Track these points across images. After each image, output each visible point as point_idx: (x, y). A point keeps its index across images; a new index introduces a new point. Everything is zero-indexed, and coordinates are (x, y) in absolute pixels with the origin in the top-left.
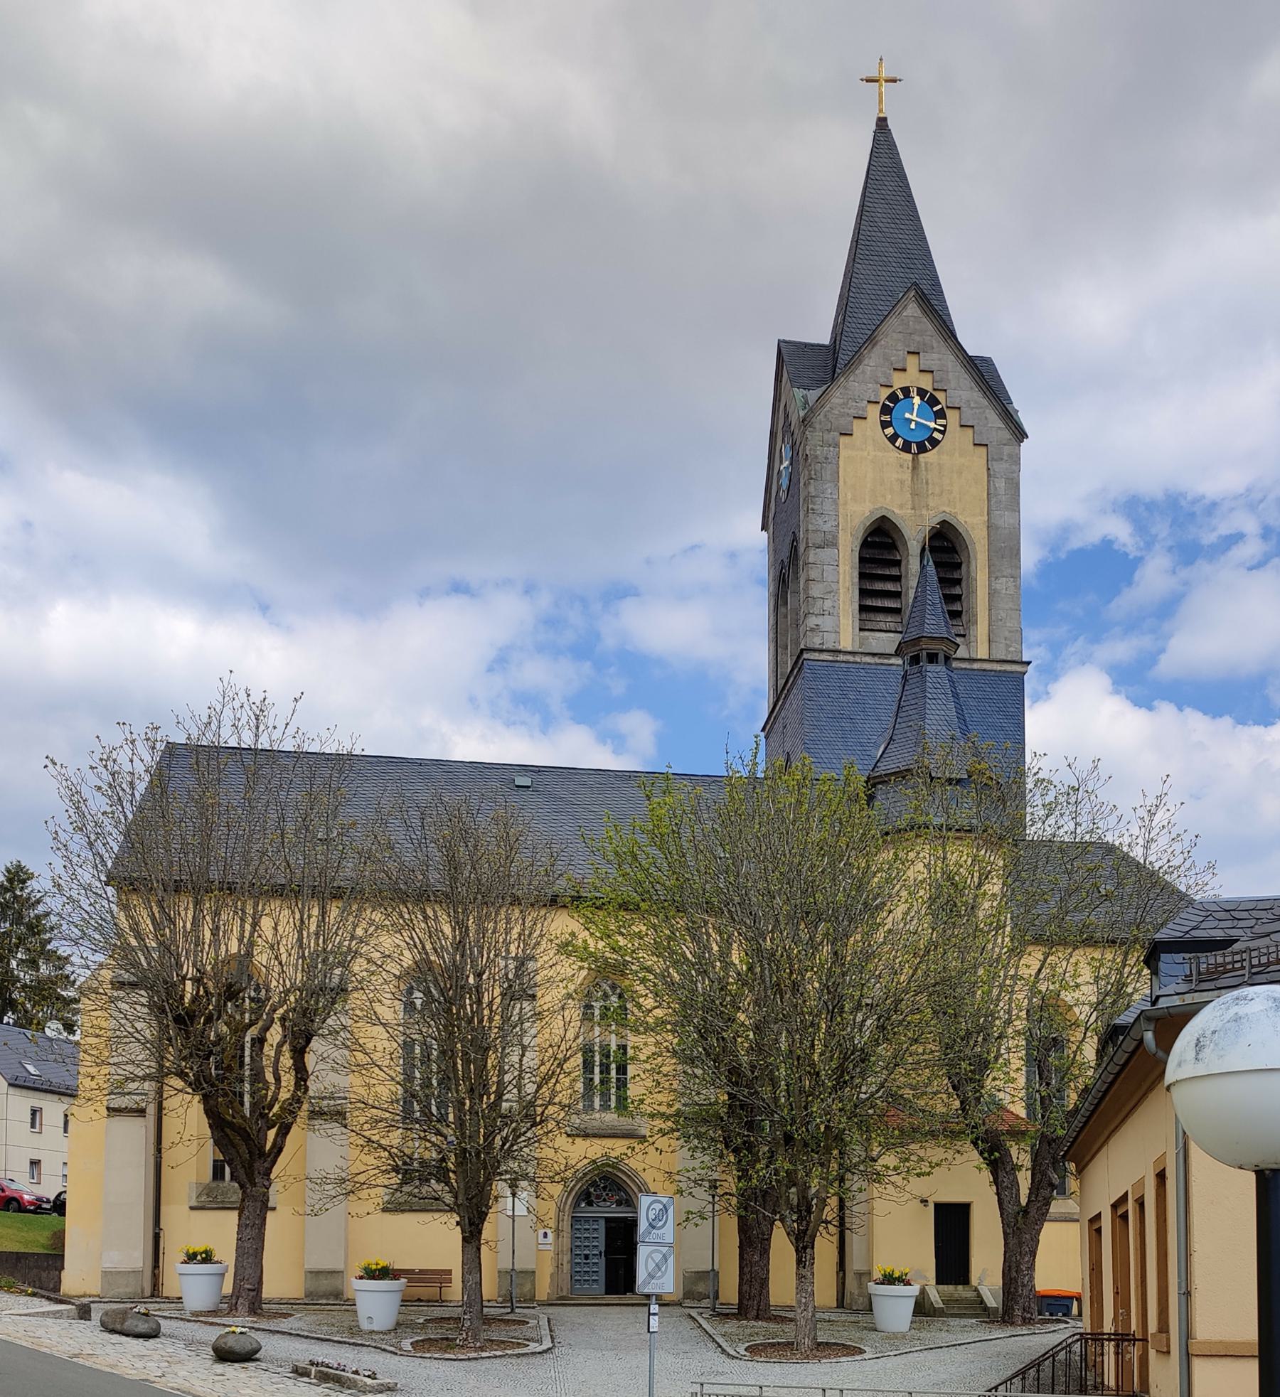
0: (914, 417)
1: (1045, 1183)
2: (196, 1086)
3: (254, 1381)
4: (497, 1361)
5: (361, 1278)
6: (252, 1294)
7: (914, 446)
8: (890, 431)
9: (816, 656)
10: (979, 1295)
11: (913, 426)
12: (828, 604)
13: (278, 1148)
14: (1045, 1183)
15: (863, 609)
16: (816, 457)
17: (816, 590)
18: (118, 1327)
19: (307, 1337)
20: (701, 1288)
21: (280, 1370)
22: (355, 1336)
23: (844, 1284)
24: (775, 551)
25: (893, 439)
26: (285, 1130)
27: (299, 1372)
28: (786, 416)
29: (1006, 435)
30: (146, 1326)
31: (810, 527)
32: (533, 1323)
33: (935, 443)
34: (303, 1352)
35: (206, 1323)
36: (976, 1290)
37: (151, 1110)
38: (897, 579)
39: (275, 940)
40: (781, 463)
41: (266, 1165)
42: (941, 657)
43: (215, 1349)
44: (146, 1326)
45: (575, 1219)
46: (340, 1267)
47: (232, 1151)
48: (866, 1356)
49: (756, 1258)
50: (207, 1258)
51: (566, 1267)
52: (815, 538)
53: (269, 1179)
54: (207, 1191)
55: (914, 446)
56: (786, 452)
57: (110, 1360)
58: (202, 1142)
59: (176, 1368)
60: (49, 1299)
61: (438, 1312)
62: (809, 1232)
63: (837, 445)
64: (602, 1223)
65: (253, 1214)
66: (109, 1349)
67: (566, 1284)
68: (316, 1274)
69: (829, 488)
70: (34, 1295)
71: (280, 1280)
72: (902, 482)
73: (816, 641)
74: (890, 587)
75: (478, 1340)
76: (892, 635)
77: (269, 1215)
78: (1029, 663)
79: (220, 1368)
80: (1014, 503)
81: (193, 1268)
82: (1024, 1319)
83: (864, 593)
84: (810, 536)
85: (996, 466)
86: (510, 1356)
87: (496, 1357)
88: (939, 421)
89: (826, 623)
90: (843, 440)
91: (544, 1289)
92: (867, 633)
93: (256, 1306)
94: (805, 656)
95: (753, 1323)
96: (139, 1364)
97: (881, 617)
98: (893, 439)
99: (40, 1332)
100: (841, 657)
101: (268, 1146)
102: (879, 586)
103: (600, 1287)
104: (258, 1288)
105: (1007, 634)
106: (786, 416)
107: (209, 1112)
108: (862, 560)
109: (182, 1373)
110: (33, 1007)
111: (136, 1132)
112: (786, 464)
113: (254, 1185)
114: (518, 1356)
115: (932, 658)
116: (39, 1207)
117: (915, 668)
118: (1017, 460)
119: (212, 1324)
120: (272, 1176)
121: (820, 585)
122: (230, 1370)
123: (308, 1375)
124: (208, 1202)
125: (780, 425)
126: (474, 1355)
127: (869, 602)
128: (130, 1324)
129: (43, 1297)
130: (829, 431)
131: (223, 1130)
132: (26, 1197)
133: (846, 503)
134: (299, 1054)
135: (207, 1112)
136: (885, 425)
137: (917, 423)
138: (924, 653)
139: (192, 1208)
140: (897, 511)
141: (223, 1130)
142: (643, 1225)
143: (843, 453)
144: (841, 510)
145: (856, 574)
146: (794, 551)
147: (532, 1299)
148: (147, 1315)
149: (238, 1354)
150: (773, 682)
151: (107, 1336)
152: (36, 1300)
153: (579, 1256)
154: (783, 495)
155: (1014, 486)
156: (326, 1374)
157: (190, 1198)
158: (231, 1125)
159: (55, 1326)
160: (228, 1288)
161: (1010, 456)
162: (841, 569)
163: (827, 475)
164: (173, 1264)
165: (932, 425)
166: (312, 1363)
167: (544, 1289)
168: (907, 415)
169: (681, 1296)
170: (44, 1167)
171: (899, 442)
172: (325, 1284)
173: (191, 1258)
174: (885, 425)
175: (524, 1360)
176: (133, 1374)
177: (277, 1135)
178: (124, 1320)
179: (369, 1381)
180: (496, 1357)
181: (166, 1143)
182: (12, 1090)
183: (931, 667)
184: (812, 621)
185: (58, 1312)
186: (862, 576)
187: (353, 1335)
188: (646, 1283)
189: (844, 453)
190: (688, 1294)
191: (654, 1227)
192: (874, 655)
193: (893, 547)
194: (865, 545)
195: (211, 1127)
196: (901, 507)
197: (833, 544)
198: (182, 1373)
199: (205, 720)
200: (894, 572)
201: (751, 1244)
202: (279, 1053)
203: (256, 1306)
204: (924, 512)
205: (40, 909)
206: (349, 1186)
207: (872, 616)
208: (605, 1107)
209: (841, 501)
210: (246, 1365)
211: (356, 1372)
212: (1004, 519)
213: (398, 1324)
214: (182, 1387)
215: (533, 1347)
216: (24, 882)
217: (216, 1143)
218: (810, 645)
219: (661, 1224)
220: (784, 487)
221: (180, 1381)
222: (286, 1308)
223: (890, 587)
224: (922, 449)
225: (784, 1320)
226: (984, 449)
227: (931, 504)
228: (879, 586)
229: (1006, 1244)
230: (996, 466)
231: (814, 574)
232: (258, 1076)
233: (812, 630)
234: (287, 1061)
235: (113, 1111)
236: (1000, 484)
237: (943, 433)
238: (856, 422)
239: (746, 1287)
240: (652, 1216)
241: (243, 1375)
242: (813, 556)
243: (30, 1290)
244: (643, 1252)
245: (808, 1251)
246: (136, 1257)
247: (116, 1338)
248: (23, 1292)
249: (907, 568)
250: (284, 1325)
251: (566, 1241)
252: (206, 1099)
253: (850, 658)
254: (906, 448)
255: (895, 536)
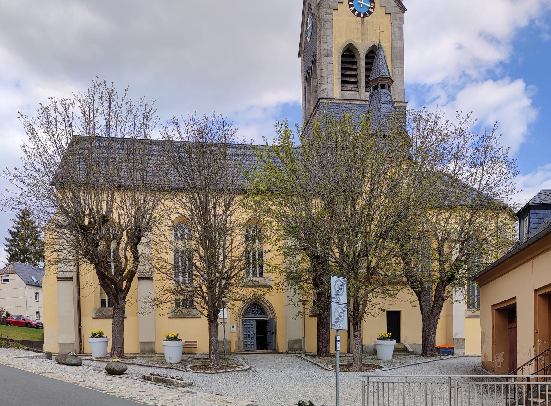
0: (362, 2)
1: (440, 299)
2: (91, 260)
3: (126, 383)
4: (230, 373)
5: (166, 341)
6: (120, 349)
7: (362, 14)
8: (352, 8)
9: (325, 101)
10: (405, 347)
11: (361, 6)
12: (329, 79)
13: (128, 288)
14: (440, 299)
15: (343, 82)
16: (324, 19)
17: (324, 74)
18: (63, 361)
19: (145, 366)
20: (295, 346)
21: (136, 378)
22: (164, 364)
23: (350, 344)
24: (305, 64)
25: (354, 12)
26: (130, 280)
27: (146, 378)
28: (310, 6)
29: (398, 10)
30: (75, 361)
31: (322, 48)
32: (235, 359)
33: (370, 13)
34: (147, 371)
35: (101, 361)
36: (403, 345)
37: (75, 279)
38: (355, 69)
39: (121, 211)
40: (307, 26)
41: (123, 295)
42: (386, 86)
43: (107, 369)
44: (75, 361)
45: (244, 321)
46: (154, 340)
47: (109, 289)
48: (383, 369)
49: (325, 331)
50: (101, 335)
51: (241, 339)
52: (324, 53)
53: (124, 301)
54: (99, 311)
55: (362, 14)
56: (310, 21)
57: (59, 375)
58: (96, 286)
59: (89, 378)
60: (34, 351)
61: (195, 357)
62: (359, 316)
63: (332, 14)
64: (255, 322)
65: (119, 320)
66: (59, 370)
67: (241, 346)
68: (144, 343)
69: (329, 32)
70: (28, 350)
71: (130, 347)
72: (357, 29)
73: (325, 95)
74: (353, 73)
75: (218, 365)
76: (354, 92)
77: (125, 320)
78: (407, 102)
79: (109, 377)
80: (401, 38)
81: (95, 339)
82: (432, 355)
83: (343, 75)
84: (322, 51)
85: (394, 22)
86: (234, 371)
87: (228, 372)
88: (372, 4)
89: (329, 87)
90: (334, 12)
91: (233, 348)
92: (344, 92)
93: (122, 355)
94: (321, 101)
95: (325, 358)
96: (72, 376)
97: (349, 85)
98: (354, 12)
99: (29, 364)
100: (335, 101)
101: (123, 288)
102: (349, 73)
103: (255, 347)
104: (122, 347)
105: (399, 91)
106: (310, 6)
107: (99, 272)
108: (342, 62)
109: (92, 380)
110: (35, 259)
111: (69, 287)
112: (310, 26)
113: (119, 304)
114: (238, 371)
115: (383, 86)
116: (38, 326)
117: (376, 91)
118: (402, 20)
119: (104, 362)
120: (126, 300)
121: (326, 72)
122: (114, 378)
123: (150, 380)
124: (99, 316)
125: (306, 12)
126: (219, 371)
127: (345, 79)
128: (69, 360)
129: (31, 350)
130: (329, 8)
131: (104, 280)
132: (33, 322)
133: (335, 38)
134: (134, 247)
135: (97, 273)
136: (350, 6)
137: (363, 5)
138: (380, 84)
139: (93, 318)
140: (356, 41)
141: (104, 280)
142: (333, 293)
143: (334, 18)
144: (334, 41)
145: (340, 67)
146: (314, 62)
147: (230, 352)
148: (75, 356)
149: (117, 371)
150: (304, 116)
151: (59, 365)
152: (28, 352)
153: (246, 335)
154: (308, 40)
155: (401, 30)
156: (159, 379)
157: (92, 314)
158: (108, 278)
159: (35, 362)
160: (109, 350)
161: (400, 18)
162: (334, 65)
163: (328, 26)
164: (87, 338)
165: (369, 6)
166: (151, 374)
167: (233, 348)
168: (359, 2)
169: (288, 349)
170: (41, 314)
171: (356, 13)
172: (148, 347)
173: (94, 335)
174: (350, 6)
175: (241, 373)
176: (69, 381)
177: (127, 282)
178: (66, 359)
179: (180, 382)
180: (228, 372)
181: (81, 287)
182: (27, 286)
183: (383, 91)
184: (323, 87)
185: (37, 356)
186: (343, 69)
187: (164, 364)
188: (335, 324)
189: (335, 18)
190: (291, 349)
191: (338, 294)
192: (347, 100)
193: (353, 56)
194: (343, 56)
195: (99, 279)
196: (357, 39)
197: (331, 54)
198: (92, 380)
199: (86, 94)
200: (354, 67)
201: (323, 326)
202: (126, 250)
203: (122, 355)
204: (366, 42)
205: (34, 225)
206: (157, 303)
207: (346, 85)
208: (254, 275)
209: (334, 37)
210: (121, 376)
211: (173, 378)
212: (397, 44)
213: (182, 361)
214: (92, 386)
215: (242, 368)
216: (28, 215)
217: (102, 285)
218: (322, 97)
219: (341, 293)
220: (309, 36)
221: (91, 383)
222: (133, 356)
223: (353, 73)
224: (365, 16)
225: (333, 356)
226: (389, 15)
227: (369, 38)
228: (349, 73)
229: (424, 324)
230: (394, 22)
231: (324, 67)
232: (117, 257)
233: (323, 90)
234: (129, 254)
235: (59, 278)
236: (396, 30)
237: (373, 9)
238: (339, 5)
239: (321, 344)
240: (337, 289)
241: (120, 380)
242: (323, 60)
243: (26, 348)
244: (333, 307)
245: (359, 324)
246: (72, 338)
247: (62, 366)
248: (23, 349)
249: (360, 65)
250: (134, 361)
251: (241, 329)
252: (96, 265)
253: (338, 101)
254: (359, 15)
255: (355, 52)
